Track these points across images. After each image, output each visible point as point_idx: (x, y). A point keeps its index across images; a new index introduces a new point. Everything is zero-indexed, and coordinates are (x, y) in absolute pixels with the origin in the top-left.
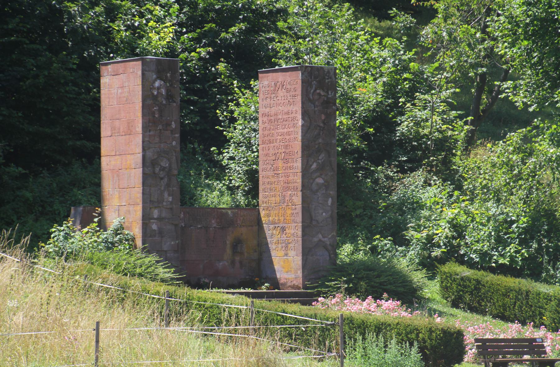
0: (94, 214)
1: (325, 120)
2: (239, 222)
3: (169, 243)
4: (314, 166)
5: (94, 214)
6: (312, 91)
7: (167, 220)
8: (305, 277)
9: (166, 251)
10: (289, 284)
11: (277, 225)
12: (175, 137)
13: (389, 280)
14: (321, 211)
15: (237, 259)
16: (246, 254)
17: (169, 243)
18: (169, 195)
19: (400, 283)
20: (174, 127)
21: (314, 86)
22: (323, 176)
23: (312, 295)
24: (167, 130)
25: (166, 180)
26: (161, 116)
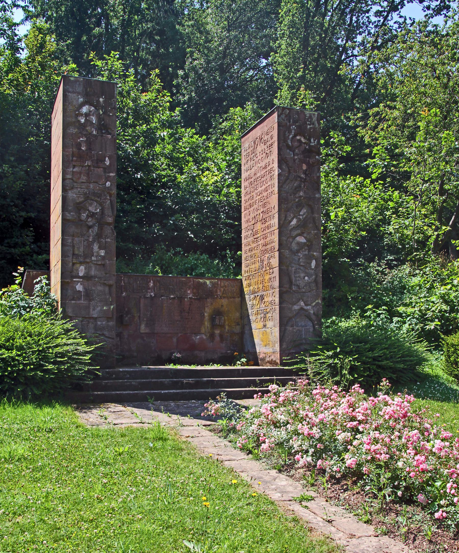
0: (14, 274)
1: (306, 170)
2: (219, 293)
3: (99, 308)
4: (294, 222)
5: (14, 274)
6: (291, 136)
7: (97, 279)
8: (282, 352)
9: (96, 319)
10: (267, 359)
11: (256, 295)
12: (109, 176)
13: (385, 354)
14: (302, 275)
15: (217, 332)
16: (227, 327)
17: (99, 308)
18: (100, 248)
19: (399, 358)
20: (108, 164)
21: (293, 131)
22: (305, 235)
23: (290, 373)
24: (99, 167)
25: (96, 228)
26: (89, 149)
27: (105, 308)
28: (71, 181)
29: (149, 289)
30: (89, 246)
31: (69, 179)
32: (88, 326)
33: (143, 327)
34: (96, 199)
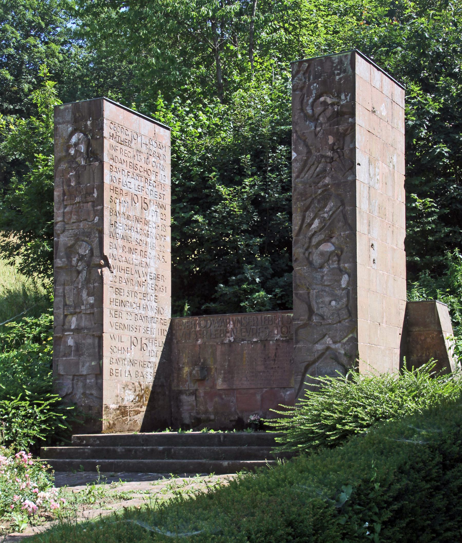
1: (334, 144)
4: (316, 224)
6: (311, 100)
7: (86, 331)
14: (327, 299)
18: (89, 295)
21: (314, 92)
22: (333, 240)
25: (84, 273)
26: (78, 183)
27: (93, 363)
28: (63, 223)
29: (228, 332)
31: (61, 221)
32: (77, 384)
34: (86, 239)
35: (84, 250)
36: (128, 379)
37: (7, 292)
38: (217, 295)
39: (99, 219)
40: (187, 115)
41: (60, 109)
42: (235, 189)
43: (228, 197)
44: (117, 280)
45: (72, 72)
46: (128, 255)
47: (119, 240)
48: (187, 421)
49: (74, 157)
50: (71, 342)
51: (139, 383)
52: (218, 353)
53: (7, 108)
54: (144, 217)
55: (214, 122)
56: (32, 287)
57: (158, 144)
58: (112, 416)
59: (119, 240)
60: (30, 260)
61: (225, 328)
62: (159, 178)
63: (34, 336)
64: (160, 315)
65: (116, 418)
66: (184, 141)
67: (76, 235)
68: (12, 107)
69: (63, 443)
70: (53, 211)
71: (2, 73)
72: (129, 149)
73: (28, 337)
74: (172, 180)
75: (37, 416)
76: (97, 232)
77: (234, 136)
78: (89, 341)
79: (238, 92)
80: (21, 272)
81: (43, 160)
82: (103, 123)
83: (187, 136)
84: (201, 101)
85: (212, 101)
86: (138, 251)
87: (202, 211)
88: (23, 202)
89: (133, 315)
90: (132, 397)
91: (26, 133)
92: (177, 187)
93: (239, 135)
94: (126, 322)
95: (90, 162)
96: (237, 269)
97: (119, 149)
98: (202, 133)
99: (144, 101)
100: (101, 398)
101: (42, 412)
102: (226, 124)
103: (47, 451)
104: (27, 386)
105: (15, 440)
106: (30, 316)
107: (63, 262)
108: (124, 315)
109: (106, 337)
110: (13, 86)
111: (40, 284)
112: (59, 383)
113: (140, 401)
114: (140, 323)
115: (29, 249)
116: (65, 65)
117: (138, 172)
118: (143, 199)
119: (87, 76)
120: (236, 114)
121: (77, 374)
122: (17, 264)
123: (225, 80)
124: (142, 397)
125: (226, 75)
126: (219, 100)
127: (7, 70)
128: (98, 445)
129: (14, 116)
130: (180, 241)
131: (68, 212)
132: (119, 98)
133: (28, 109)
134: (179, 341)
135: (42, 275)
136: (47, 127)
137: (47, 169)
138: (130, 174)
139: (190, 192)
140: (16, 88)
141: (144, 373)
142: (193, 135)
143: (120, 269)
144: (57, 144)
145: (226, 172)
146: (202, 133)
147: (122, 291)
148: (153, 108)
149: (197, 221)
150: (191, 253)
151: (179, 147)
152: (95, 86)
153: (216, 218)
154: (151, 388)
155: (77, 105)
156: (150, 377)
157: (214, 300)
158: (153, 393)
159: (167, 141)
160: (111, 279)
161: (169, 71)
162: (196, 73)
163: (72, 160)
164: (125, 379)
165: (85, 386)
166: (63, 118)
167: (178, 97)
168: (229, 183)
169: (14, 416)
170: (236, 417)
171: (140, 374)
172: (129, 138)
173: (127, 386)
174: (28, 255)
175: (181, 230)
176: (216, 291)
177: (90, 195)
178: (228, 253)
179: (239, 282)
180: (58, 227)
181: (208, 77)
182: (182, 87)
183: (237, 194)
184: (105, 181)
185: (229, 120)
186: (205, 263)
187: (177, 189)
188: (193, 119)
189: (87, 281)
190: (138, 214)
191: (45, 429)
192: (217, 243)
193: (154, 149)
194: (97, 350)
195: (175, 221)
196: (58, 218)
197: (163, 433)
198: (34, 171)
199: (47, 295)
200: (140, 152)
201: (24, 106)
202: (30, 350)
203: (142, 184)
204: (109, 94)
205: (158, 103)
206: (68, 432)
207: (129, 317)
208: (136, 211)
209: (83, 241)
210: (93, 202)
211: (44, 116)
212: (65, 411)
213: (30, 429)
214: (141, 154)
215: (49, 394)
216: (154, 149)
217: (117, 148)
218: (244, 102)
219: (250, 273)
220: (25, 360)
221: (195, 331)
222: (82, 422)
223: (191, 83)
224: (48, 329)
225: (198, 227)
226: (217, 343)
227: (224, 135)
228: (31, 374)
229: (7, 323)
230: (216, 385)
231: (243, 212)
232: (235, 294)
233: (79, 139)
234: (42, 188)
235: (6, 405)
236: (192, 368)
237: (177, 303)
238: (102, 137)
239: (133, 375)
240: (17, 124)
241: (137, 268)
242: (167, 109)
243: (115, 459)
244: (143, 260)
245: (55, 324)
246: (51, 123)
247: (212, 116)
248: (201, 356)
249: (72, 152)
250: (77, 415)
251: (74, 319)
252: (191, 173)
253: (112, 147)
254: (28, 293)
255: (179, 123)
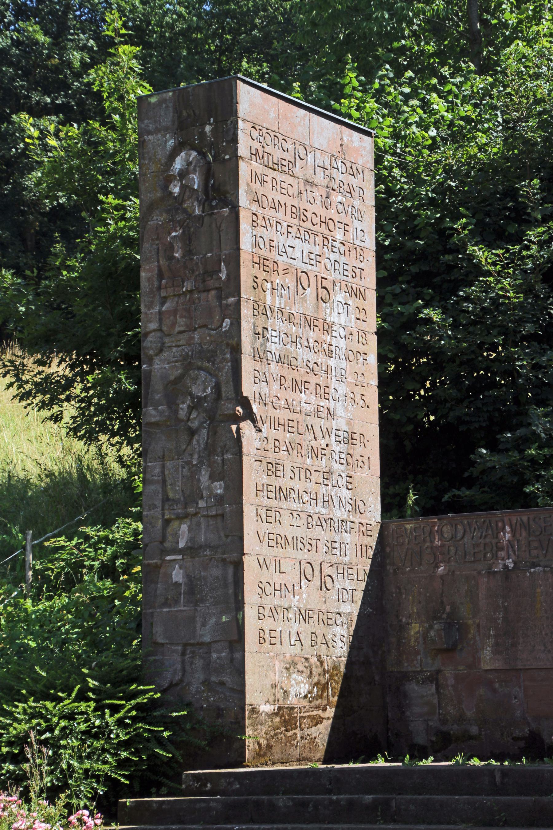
7: (208, 552)
18: (213, 478)
25: (204, 433)
26: (189, 252)
27: (224, 619)
28: (158, 334)
29: (502, 549)
30: (193, 477)
31: (154, 330)
32: (192, 663)
33: (487, 653)
34: (206, 364)
35: (201, 388)
36: (297, 649)
37: (47, 476)
38: (475, 471)
39: (231, 324)
40: (406, 103)
41: (150, 103)
42: (508, 250)
43: (492, 268)
44: (270, 446)
45: (167, 23)
46: (290, 395)
47: (273, 365)
48: (421, 739)
49: (180, 200)
50: (178, 575)
51: (319, 658)
52: (482, 593)
53: (38, 103)
54: (321, 315)
55: (463, 114)
56: (96, 464)
57: (349, 165)
58: (264, 729)
59: (273, 365)
60: (92, 409)
61: (494, 541)
62: (351, 236)
63: (103, 565)
64: (358, 515)
65: (272, 733)
66: (399, 156)
67: (185, 357)
68: (49, 100)
69: (164, 790)
70: (139, 311)
71: (28, 31)
72: (290, 180)
73: (91, 567)
74: (377, 239)
75: (111, 732)
76: (228, 351)
77: (505, 140)
78: (216, 572)
79: (513, 46)
80: (75, 434)
81: (117, 208)
82: (236, 128)
83: (406, 146)
84: (435, 73)
85: (457, 71)
86: (312, 387)
87: (439, 299)
88: (76, 294)
89: (304, 516)
90: (304, 689)
91: (80, 154)
92: (386, 253)
93: (515, 139)
94: (290, 533)
95: (212, 208)
96: (515, 417)
97: (268, 179)
98: (438, 139)
99: (315, 79)
100: (242, 692)
101: (120, 723)
102: (488, 116)
103: (130, 807)
104: (90, 669)
105: (66, 786)
106: (94, 524)
107: (161, 413)
108: (286, 518)
109: (249, 563)
110: (49, 57)
111: (113, 456)
112: (155, 661)
113: (321, 697)
114: (317, 532)
115: (89, 388)
116: (153, 8)
117: (308, 225)
118: (320, 279)
119: (199, 29)
120: (509, 94)
121: (192, 641)
122: (67, 418)
123: (485, 23)
124: (324, 687)
125: (488, 13)
126: (472, 67)
127: (36, 23)
128: (237, 793)
129: (54, 118)
130: (395, 362)
131: (168, 312)
132: (264, 74)
133: (81, 103)
134: (398, 568)
135: (117, 439)
136: (123, 140)
137: (125, 226)
138: (293, 230)
139: (414, 262)
140: (56, 61)
141: (329, 637)
142: (418, 144)
143: (276, 424)
144: (145, 175)
145: (489, 216)
146: (438, 139)
147: (281, 468)
148: (336, 92)
149: (429, 320)
150: (418, 386)
151: (390, 169)
152: (215, 51)
153: (468, 312)
154: (342, 669)
155: (182, 95)
156: (340, 644)
157: (470, 483)
158: (346, 677)
159: (366, 160)
160: (257, 444)
161: (368, 11)
162: (424, 14)
163: (175, 205)
164: (290, 651)
165: (207, 666)
166: (155, 122)
167: (387, 66)
168: (495, 240)
169: (65, 733)
170: (527, 730)
171: (320, 640)
172: (288, 157)
173: (294, 664)
174: (88, 401)
175: (391, 340)
176: (473, 464)
177: (212, 276)
178: (495, 385)
179: (521, 444)
180: (150, 343)
181: (449, 20)
182: (396, 45)
183: (513, 262)
184: (242, 246)
185: (495, 108)
186: (448, 405)
187: (387, 257)
188: (419, 110)
189: (210, 449)
190: (310, 311)
191: (127, 759)
192: (472, 365)
193: (341, 177)
194: (231, 591)
195: (383, 321)
196: (149, 324)
197: (371, 764)
198: (99, 229)
199: (128, 478)
200: (312, 184)
201: (73, 96)
202: (95, 594)
203: (317, 250)
204: (245, 64)
205: (347, 80)
206: (175, 765)
207: (295, 522)
208: (307, 304)
209: (200, 368)
210: (219, 289)
211: (117, 117)
212: (168, 720)
213: (98, 760)
214: (314, 189)
215: (135, 686)
216: (341, 177)
217: (266, 178)
218: (525, 67)
219: (544, 425)
220: (86, 615)
221: (432, 548)
222: (204, 743)
223: (414, 34)
224: (131, 549)
225: (433, 333)
226: (479, 573)
227: (484, 141)
228: (96, 644)
229: (48, 539)
230: (479, 662)
231: (526, 299)
232: (513, 468)
233: (189, 164)
234: (115, 263)
235: (47, 709)
236: (426, 625)
237: (391, 490)
238: (236, 157)
239: (307, 641)
240: (62, 135)
241: (310, 420)
242: (364, 91)
243: (273, 822)
244: (322, 404)
245: (147, 540)
246: (130, 132)
247: (459, 102)
248: (445, 600)
249: (176, 190)
250: (193, 729)
251: (184, 528)
252: (416, 223)
253: (254, 175)
254: (89, 477)
255: (390, 121)
